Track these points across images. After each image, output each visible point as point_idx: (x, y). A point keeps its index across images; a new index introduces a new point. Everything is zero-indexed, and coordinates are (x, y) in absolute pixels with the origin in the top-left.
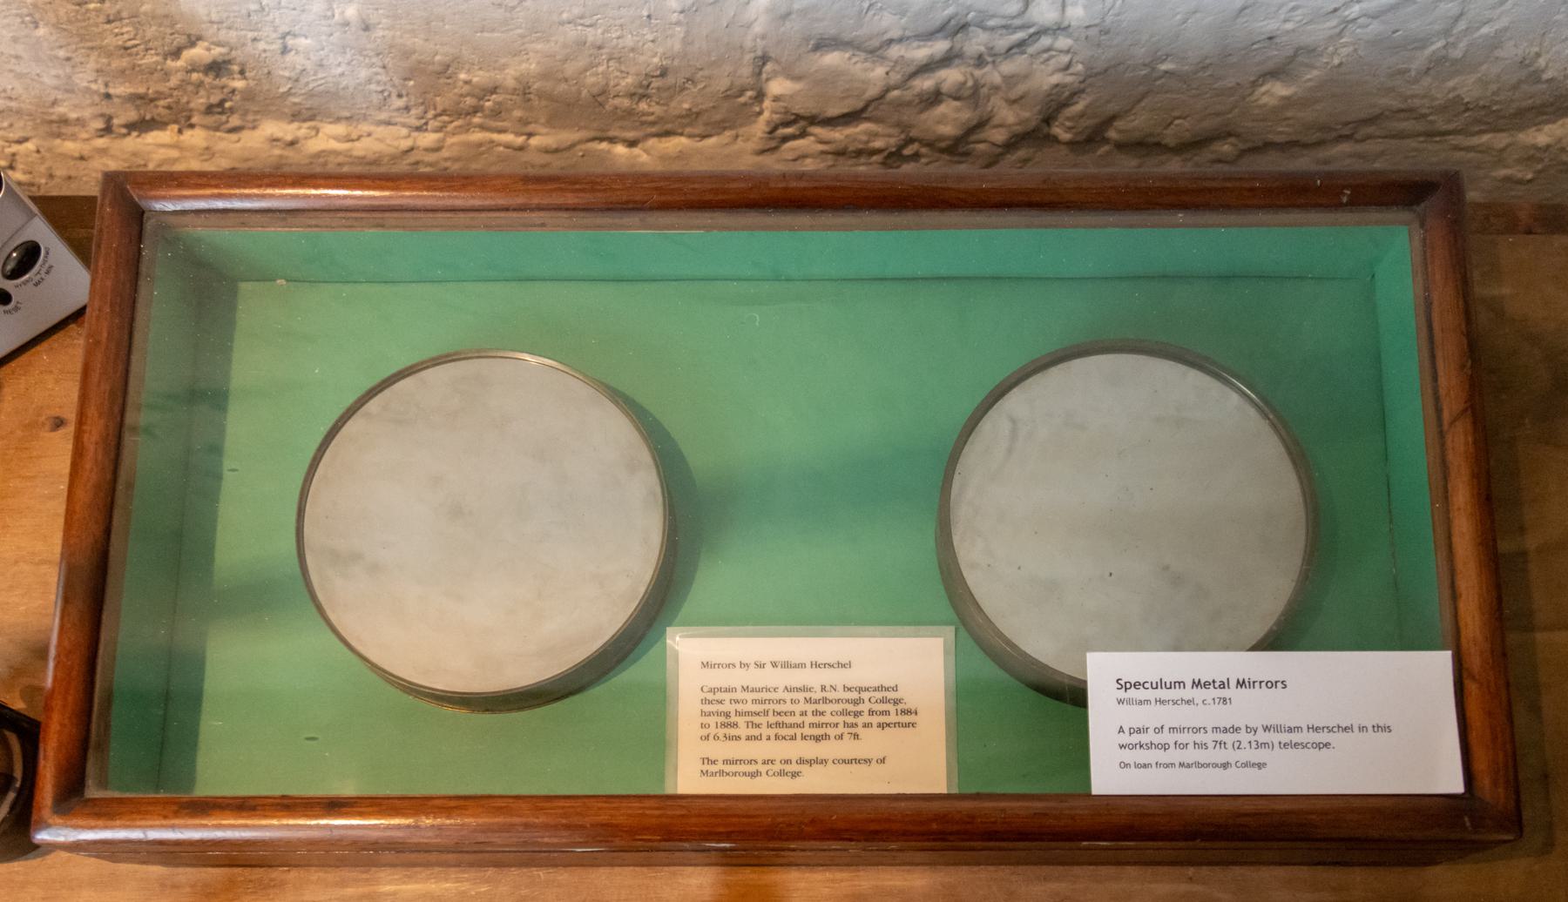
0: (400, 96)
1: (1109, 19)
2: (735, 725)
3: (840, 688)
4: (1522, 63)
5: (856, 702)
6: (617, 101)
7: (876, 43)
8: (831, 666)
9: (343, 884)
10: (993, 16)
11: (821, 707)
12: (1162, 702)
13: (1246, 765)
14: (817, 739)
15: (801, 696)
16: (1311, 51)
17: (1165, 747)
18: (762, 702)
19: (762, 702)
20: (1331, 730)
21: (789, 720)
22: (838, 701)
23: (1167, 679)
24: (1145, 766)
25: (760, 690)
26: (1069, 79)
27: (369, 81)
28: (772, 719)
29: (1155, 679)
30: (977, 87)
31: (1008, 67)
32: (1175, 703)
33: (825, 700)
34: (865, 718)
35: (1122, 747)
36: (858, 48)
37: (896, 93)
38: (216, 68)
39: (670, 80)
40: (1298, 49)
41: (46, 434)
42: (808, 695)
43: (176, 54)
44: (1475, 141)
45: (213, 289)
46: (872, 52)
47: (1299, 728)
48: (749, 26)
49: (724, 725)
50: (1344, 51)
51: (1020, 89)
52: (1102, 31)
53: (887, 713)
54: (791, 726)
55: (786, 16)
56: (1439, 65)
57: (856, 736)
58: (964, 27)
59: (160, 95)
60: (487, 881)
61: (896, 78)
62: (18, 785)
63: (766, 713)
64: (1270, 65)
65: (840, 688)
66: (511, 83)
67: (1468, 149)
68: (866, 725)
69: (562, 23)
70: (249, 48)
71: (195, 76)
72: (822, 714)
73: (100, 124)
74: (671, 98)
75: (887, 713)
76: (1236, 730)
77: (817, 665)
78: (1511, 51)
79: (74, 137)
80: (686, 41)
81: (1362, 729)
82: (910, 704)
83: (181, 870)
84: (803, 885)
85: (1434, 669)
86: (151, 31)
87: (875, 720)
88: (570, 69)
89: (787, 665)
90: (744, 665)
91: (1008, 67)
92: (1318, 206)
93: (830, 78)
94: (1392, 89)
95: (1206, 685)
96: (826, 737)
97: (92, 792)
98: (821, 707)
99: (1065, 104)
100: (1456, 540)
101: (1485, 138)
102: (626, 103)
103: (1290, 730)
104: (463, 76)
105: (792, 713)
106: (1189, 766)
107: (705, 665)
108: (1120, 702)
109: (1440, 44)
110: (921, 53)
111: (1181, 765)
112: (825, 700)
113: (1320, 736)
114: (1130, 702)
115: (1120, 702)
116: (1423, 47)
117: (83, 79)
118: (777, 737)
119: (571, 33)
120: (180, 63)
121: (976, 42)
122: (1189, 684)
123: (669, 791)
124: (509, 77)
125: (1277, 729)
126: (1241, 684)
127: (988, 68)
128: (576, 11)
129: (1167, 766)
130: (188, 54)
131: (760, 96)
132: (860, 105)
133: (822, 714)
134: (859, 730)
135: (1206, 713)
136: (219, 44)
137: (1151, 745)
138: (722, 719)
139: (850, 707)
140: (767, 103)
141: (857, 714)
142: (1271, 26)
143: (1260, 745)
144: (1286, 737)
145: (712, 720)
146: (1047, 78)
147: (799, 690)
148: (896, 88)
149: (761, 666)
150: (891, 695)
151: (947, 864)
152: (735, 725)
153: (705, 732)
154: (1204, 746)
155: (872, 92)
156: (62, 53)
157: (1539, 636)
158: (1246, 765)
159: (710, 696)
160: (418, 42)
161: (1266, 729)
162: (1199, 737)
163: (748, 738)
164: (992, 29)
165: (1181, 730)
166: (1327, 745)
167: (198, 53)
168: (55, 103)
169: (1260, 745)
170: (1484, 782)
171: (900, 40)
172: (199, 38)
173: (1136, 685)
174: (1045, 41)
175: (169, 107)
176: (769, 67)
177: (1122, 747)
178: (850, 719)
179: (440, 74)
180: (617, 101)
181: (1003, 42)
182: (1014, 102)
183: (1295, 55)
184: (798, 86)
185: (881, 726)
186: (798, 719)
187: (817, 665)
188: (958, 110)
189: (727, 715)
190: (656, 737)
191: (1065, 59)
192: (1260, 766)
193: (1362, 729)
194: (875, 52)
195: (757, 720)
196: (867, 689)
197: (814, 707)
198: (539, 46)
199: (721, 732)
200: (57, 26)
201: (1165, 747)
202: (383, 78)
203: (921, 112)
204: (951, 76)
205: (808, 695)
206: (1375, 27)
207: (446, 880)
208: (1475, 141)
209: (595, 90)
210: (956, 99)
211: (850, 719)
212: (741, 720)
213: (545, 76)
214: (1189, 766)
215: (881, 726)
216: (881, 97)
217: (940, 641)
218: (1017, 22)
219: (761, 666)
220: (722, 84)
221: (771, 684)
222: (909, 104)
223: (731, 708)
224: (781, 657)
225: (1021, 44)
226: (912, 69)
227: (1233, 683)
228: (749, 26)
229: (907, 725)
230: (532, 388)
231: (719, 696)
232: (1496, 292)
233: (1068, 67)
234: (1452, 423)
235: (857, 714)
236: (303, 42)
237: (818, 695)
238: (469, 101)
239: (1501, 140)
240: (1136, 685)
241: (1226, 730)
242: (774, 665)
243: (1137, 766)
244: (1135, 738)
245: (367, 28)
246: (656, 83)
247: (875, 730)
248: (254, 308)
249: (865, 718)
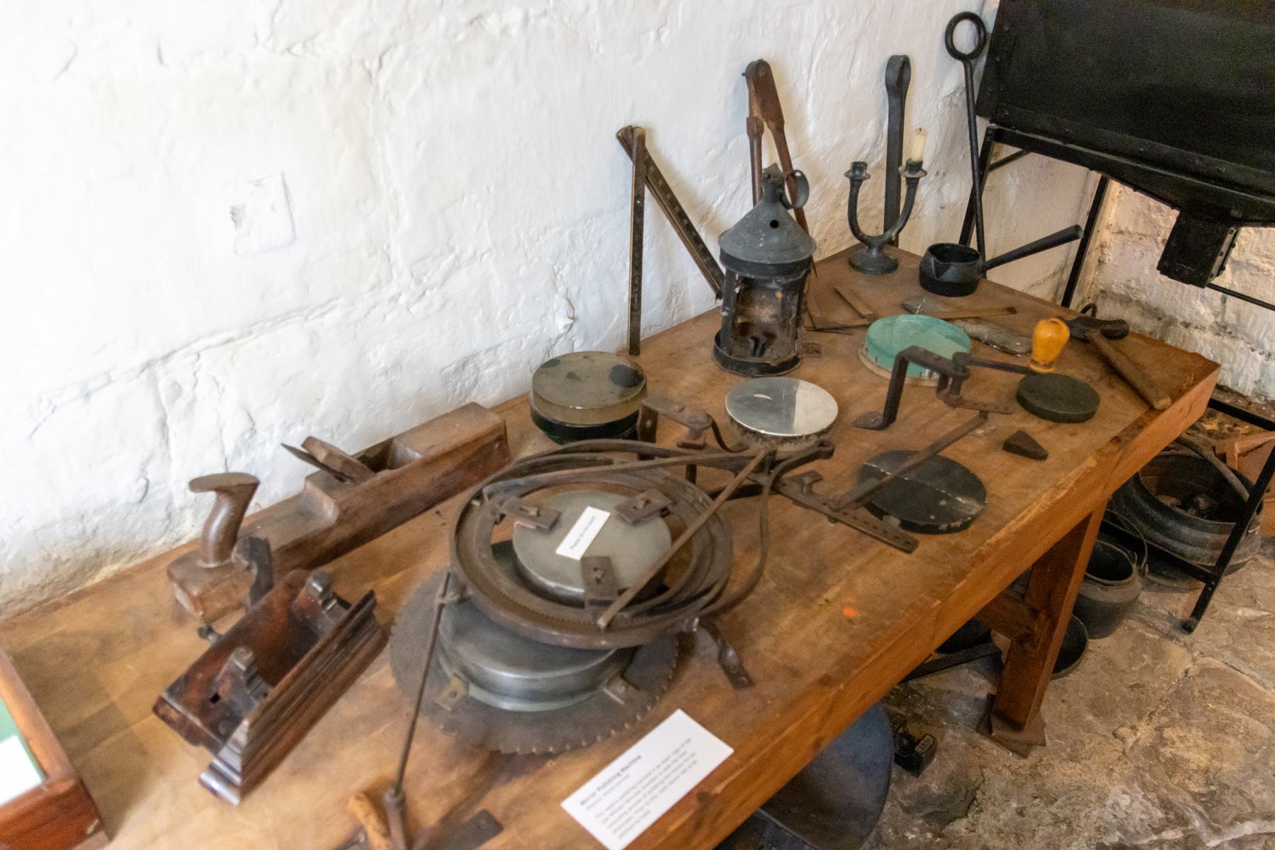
4: (47, 559)
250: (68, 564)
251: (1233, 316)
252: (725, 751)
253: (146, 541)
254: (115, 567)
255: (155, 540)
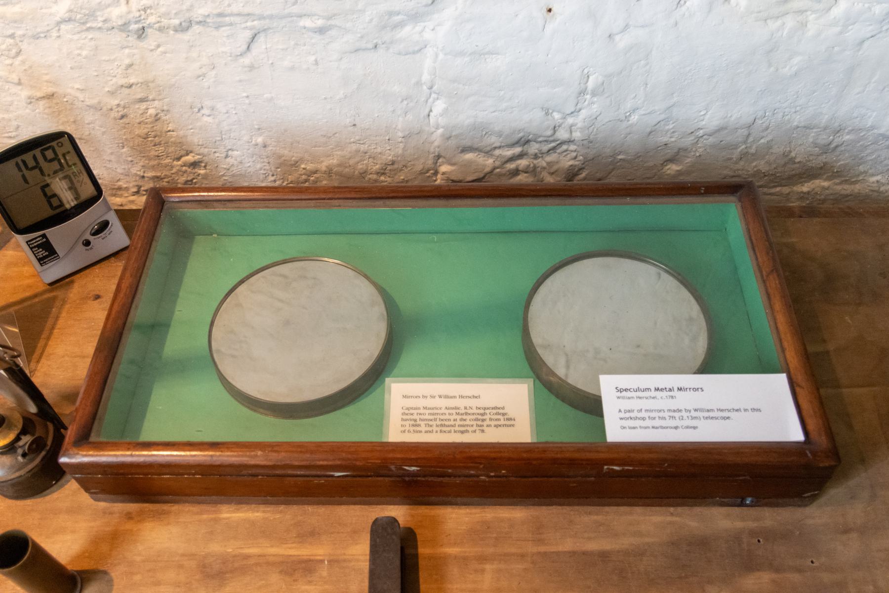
0: (273, 175)
1: (591, 137)
2: (419, 425)
3: (474, 408)
4: (785, 155)
5: (482, 415)
6: (370, 176)
7: (488, 148)
8: (470, 397)
9: (201, 513)
10: (540, 137)
11: (464, 417)
12: (640, 398)
13: (687, 427)
14: (462, 432)
15: (454, 411)
16: (685, 150)
17: (643, 419)
18: (433, 414)
19: (433, 414)
20: (729, 411)
21: (447, 423)
22: (473, 414)
23: (642, 387)
24: (634, 428)
25: (433, 409)
26: (577, 163)
27: (261, 169)
28: (439, 423)
29: (635, 387)
30: (535, 167)
31: (549, 158)
32: (647, 398)
33: (466, 414)
34: (488, 422)
35: (621, 419)
36: (481, 151)
37: (498, 170)
38: (195, 164)
39: (396, 166)
40: (680, 149)
41: (90, 302)
42: (458, 411)
43: (179, 159)
44: (773, 190)
45: (186, 235)
46: (487, 153)
47: (712, 410)
48: (432, 143)
49: (413, 425)
50: (701, 150)
51: (555, 168)
52: (589, 142)
53: (499, 420)
54: (449, 426)
55: (449, 138)
56: (744, 155)
57: (483, 431)
58: (528, 142)
59: (166, 176)
60: (281, 512)
61: (498, 163)
62: (48, 448)
63: (435, 420)
64: (668, 157)
65: (474, 408)
66: (324, 169)
67: (770, 194)
68: (488, 426)
69: (350, 143)
70: (212, 156)
71: (184, 168)
72: (465, 420)
73: (135, 190)
74: (395, 174)
75: (499, 420)
76: (680, 411)
77: (462, 397)
78: (778, 150)
79: (121, 196)
80: (404, 149)
81: (746, 410)
82: (511, 416)
83: (116, 504)
84: (454, 516)
85: (780, 381)
86: (171, 149)
87: (493, 423)
88: (352, 162)
89: (447, 397)
90: (425, 397)
91: (549, 158)
92: (690, 194)
93: (470, 163)
94: (727, 167)
95: (662, 390)
96: (467, 431)
97: (93, 438)
98: (464, 417)
99: (576, 174)
100: (779, 325)
101: (778, 189)
102: (375, 177)
103: (708, 411)
104: (303, 166)
105: (449, 420)
106: (657, 428)
107: (405, 397)
108: (618, 398)
109: (743, 147)
110: (509, 153)
111: (653, 427)
112: (466, 414)
113: (724, 414)
114: (623, 398)
115: (618, 398)
116: (736, 148)
117: (134, 170)
118: (441, 431)
119: (354, 147)
120: (180, 163)
121: (533, 148)
122: (653, 389)
123: (385, 440)
124: (323, 167)
125: (702, 410)
126: (680, 389)
127: (540, 160)
128: (357, 138)
129: (646, 428)
130: (184, 159)
131: (436, 173)
132: (482, 175)
133: (465, 420)
134: (485, 428)
135: (662, 402)
136: (199, 154)
137: (636, 418)
138: (413, 422)
139: (480, 417)
140: (439, 176)
141: (483, 420)
142: (665, 139)
143: (693, 418)
144: (706, 414)
145: (407, 423)
146: (567, 162)
147: (453, 408)
148: (498, 168)
149: (433, 397)
150: (501, 411)
151: (534, 505)
152: (419, 425)
153: (403, 429)
154: (664, 418)
155: (488, 169)
156: (130, 159)
157: (845, 391)
158: (687, 427)
159: (407, 412)
160: (286, 152)
161: (696, 410)
162: (661, 414)
163: (426, 432)
164: (541, 142)
165: (651, 411)
166: (728, 418)
167: (190, 158)
168: (119, 180)
169: (693, 418)
170: (814, 435)
171: (500, 147)
172: (191, 152)
173: (626, 390)
174: (564, 147)
175: (168, 182)
176: (440, 160)
177: (621, 419)
178: (480, 423)
179: (292, 165)
180: (370, 176)
181: (546, 148)
182: (553, 173)
183: (678, 152)
184: (453, 168)
185: (496, 426)
186: (452, 423)
187: (462, 397)
188: (527, 177)
189: (415, 420)
190: (380, 418)
191: (574, 154)
192: (695, 428)
193: (746, 410)
194: (488, 153)
195: (431, 423)
196: (488, 409)
197: (460, 417)
198: (339, 153)
199: (412, 429)
200: (132, 148)
201: (643, 419)
202: (268, 168)
203: (511, 178)
204: (523, 163)
205: (458, 411)
206: (711, 140)
207: (258, 512)
208: (773, 190)
209: (361, 171)
210: (526, 172)
211: (480, 423)
212: (422, 423)
213: (339, 165)
214: (657, 428)
215: (496, 426)
216: (491, 172)
217: (526, 385)
218: (551, 139)
219: (433, 397)
220: (419, 167)
221: (438, 406)
222: (504, 175)
223: (418, 417)
224: (443, 393)
225: (554, 148)
226: (504, 160)
227: (676, 389)
228: (432, 143)
229: (510, 426)
230: (330, 270)
231: (411, 411)
232: (790, 240)
233: (576, 158)
234: (767, 276)
235: (483, 420)
236: (235, 153)
237: (463, 411)
238: (304, 177)
239: (786, 190)
240: (626, 390)
241: (674, 411)
242: (440, 397)
243: (630, 428)
244: (628, 415)
245: (265, 146)
246: (389, 168)
247: (493, 429)
248: (200, 246)
249: (488, 422)
250: (797, 165)
251: (817, 149)
252: (796, 434)
253: (865, 172)
254: (826, 184)
255: (873, 175)
